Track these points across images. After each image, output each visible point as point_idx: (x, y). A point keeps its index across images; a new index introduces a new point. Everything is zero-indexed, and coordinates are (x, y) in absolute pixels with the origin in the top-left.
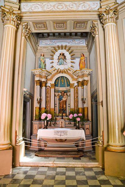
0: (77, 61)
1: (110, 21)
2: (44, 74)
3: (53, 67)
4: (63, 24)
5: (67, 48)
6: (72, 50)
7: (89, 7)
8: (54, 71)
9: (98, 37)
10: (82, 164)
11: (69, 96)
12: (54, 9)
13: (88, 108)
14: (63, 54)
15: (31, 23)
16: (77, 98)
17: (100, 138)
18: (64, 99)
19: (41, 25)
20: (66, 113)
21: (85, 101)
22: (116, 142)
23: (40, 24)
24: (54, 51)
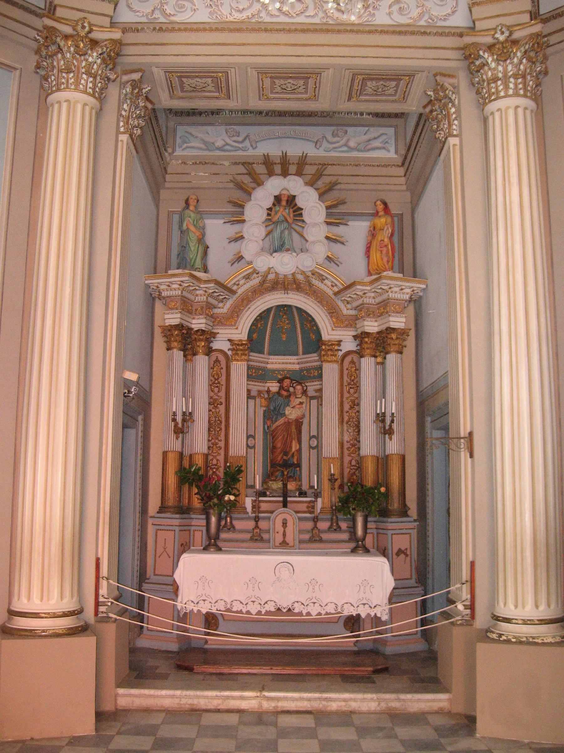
0: (357, 231)
1: (511, 92)
2: (200, 297)
3: (241, 258)
4: (301, 82)
5: (310, 170)
6: (334, 179)
7: (421, 15)
8: (248, 277)
9: (458, 148)
10: (385, 700)
11: (312, 398)
12: (263, 14)
13: (403, 458)
14: (287, 201)
15: (159, 74)
16: (351, 408)
17: (460, 589)
18: (292, 413)
19: (204, 80)
20: (300, 480)
21: (395, 426)
22: (523, 607)
23: (197, 77)
24: (247, 180)
